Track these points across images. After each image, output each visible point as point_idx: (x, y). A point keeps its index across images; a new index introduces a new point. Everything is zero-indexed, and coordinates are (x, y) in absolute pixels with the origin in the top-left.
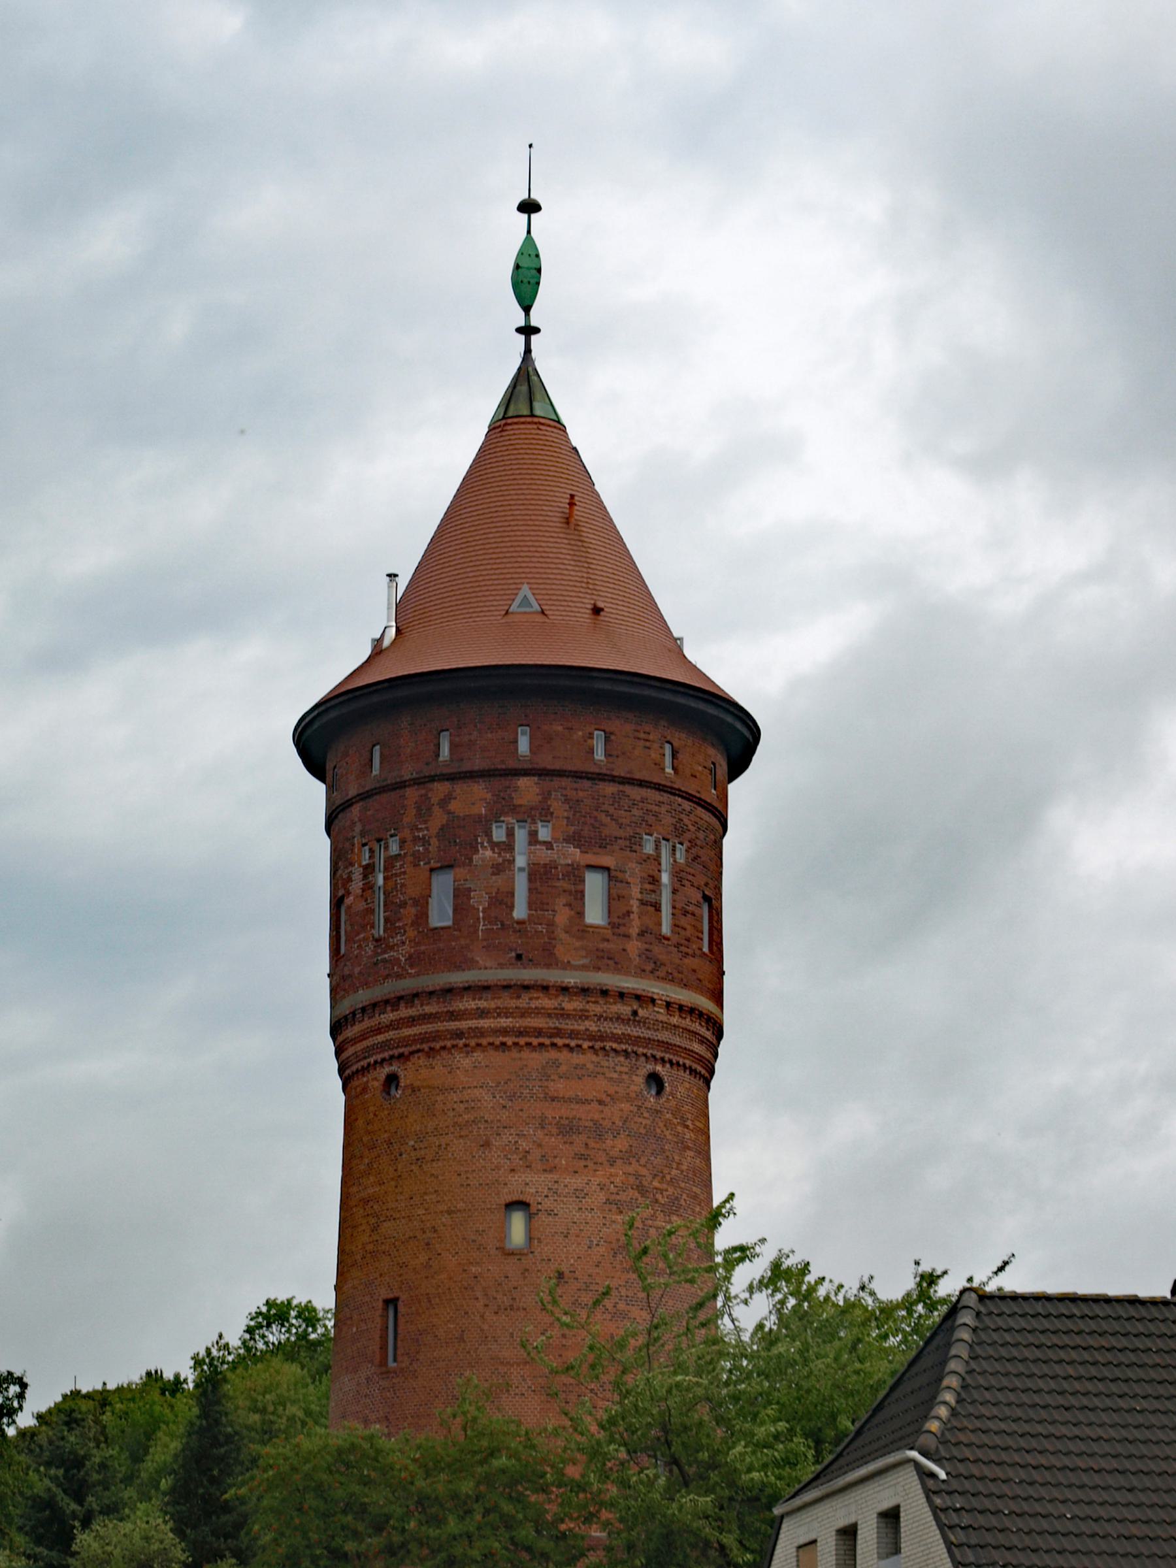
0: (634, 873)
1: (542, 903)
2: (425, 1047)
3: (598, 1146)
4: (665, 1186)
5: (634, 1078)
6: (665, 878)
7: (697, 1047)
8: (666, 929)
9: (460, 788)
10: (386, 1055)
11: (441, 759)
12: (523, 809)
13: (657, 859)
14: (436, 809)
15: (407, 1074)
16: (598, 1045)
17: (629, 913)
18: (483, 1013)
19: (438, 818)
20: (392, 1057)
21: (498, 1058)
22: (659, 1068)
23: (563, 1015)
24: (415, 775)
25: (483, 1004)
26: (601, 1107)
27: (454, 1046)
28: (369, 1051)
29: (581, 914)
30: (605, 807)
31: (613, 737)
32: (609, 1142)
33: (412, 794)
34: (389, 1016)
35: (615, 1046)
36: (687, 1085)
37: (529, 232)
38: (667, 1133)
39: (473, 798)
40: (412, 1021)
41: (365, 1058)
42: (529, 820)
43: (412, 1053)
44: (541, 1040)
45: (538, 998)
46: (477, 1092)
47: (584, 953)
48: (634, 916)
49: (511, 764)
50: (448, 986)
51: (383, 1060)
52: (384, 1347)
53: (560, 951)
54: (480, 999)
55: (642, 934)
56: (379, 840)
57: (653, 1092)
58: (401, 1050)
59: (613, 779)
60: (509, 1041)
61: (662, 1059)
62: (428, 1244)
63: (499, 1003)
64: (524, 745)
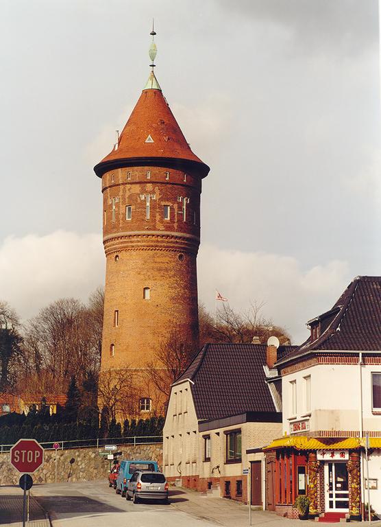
0: (176, 206)
9: (133, 186)
18: (138, 242)
19: (128, 194)
23: (158, 241)
33: (122, 187)
52: (115, 322)
59: (171, 184)
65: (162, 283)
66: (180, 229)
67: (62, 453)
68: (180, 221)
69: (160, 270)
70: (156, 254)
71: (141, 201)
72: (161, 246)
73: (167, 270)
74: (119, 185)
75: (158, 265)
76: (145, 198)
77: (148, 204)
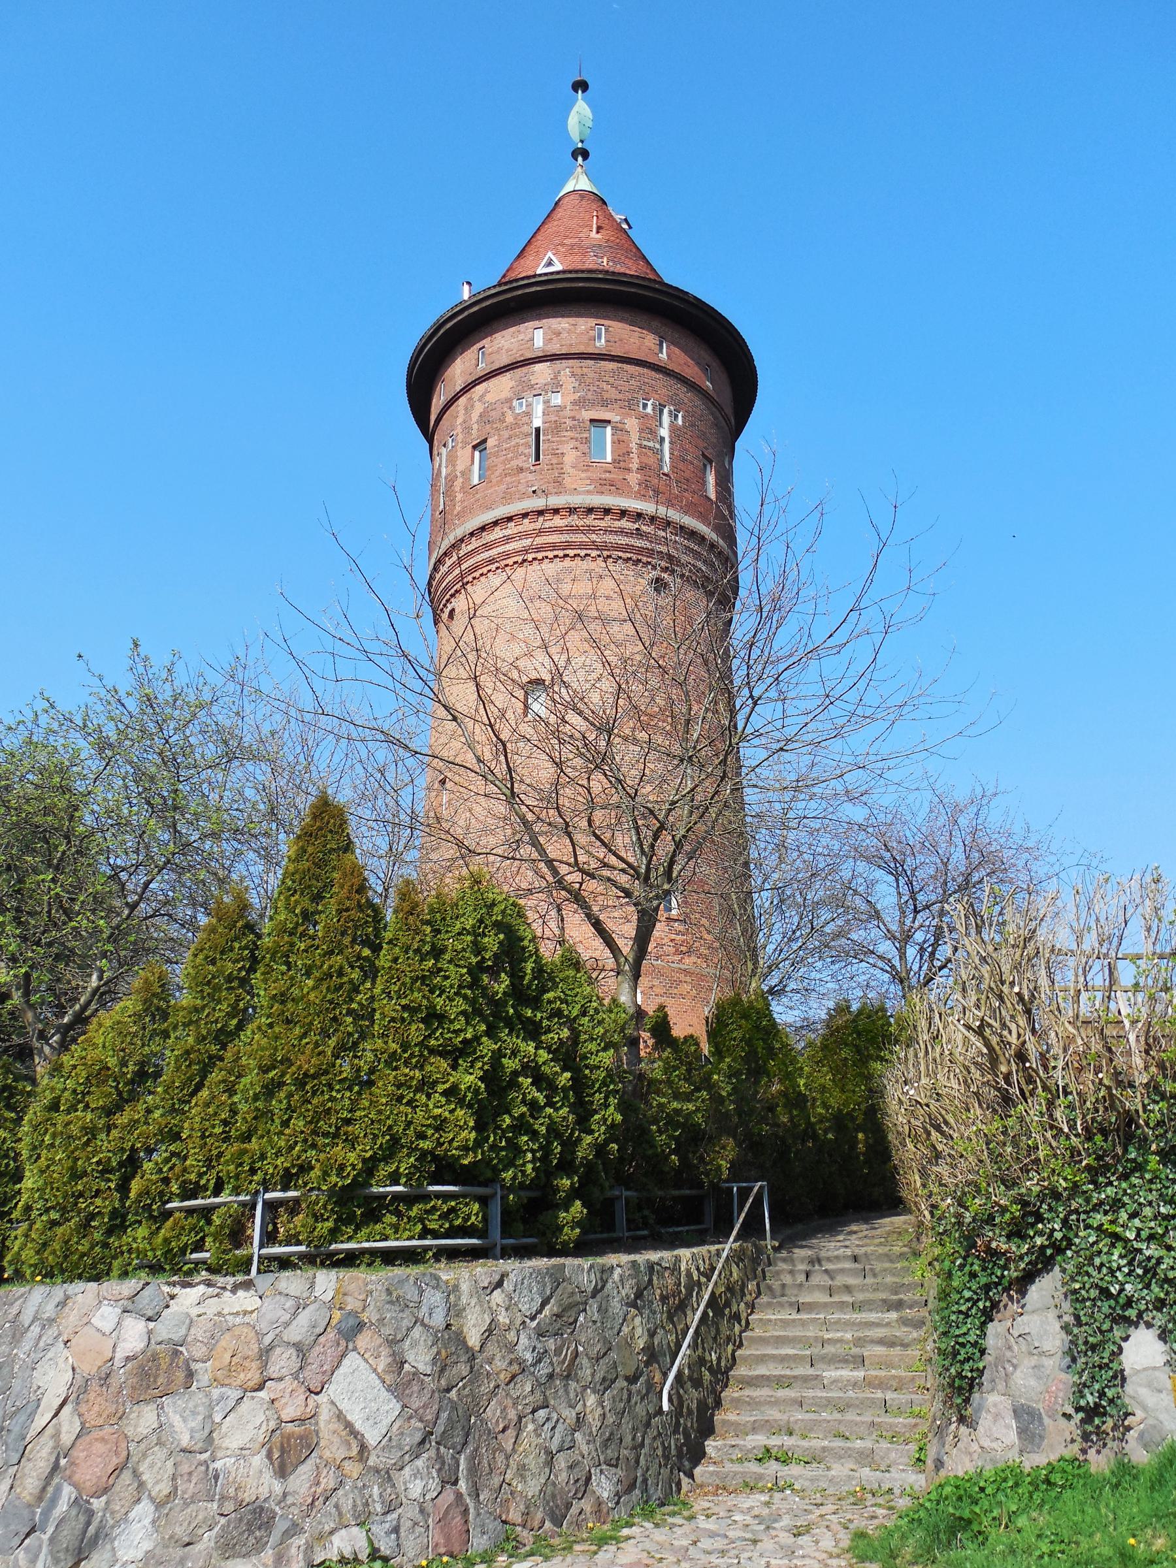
0: (632, 424)
4: (1138, 1094)
5: (640, 580)
17: (628, 453)
18: (508, 539)
30: (606, 379)
35: (620, 554)
39: (503, 385)
44: (556, 553)
47: (588, 482)
49: (529, 355)
53: (567, 481)
55: (641, 469)
63: (520, 528)
66: (650, 489)
67: (942, 1473)
71: (516, 416)
72: (582, 545)
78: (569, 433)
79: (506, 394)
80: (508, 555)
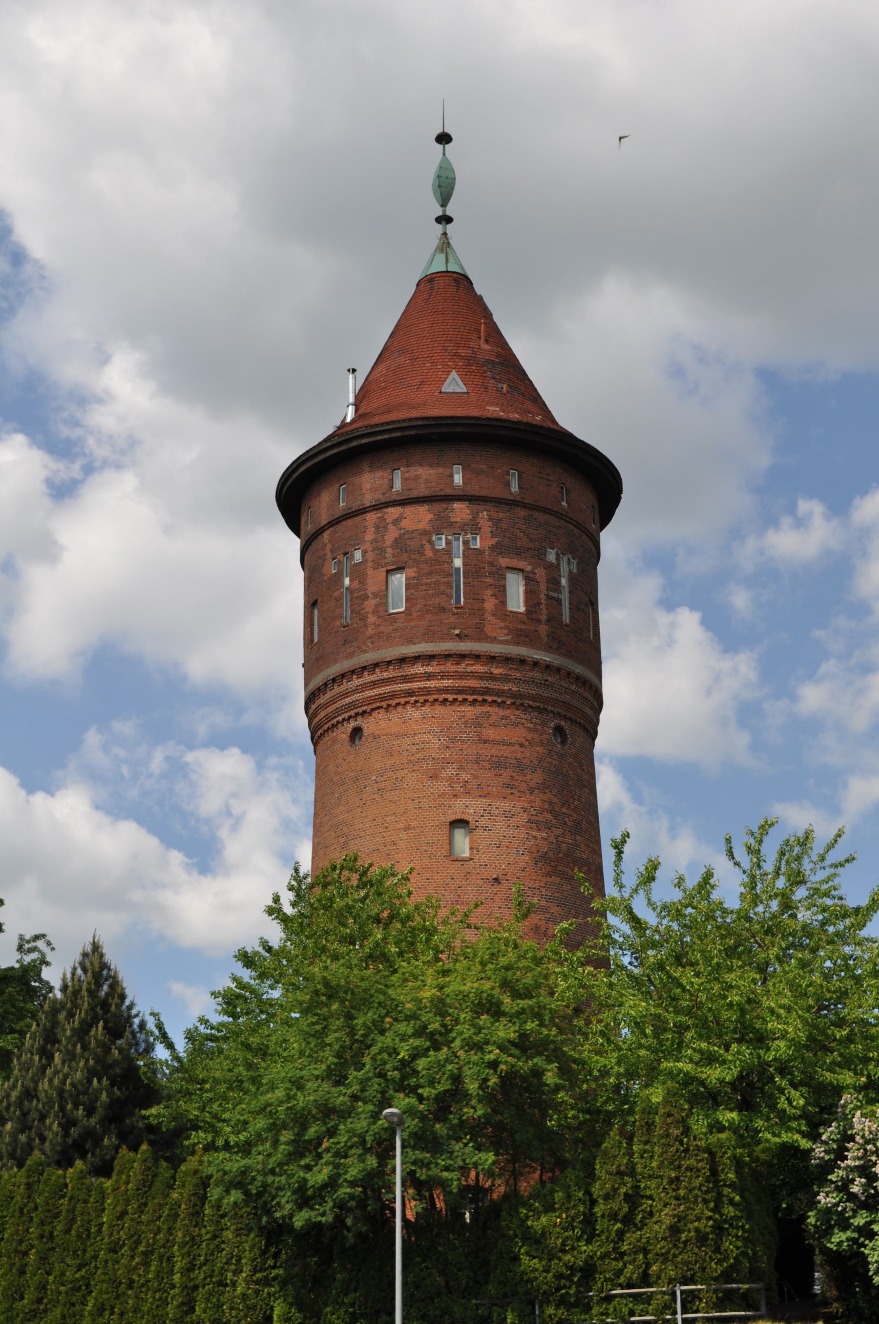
0: (541, 574)
1: (474, 594)
2: (384, 704)
3: (520, 778)
5: (545, 728)
6: (564, 582)
7: (587, 710)
8: (566, 618)
9: (409, 510)
10: (352, 713)
11: (394, 490)
12: (458, 525)
13: (557, 567)
14: (390, 526)
15: (369, 725)
16: (518, 702)
18: (429, 676)
20: (357, 714)
21: (439, 710)
22: (563, 723)
23: (491, 677)
24: (374, 503)
25: (429, 669)
26: (522, 749)
27: (407, 703)
28: (338, 712)
29: (504, 603)
31: (524, 475)
32: (529, 776)
33: (371, 518)
34: (356, 682)
35: (531, 703)
36: (582, 739)
37: (444, 154)
38: (571, 772)
40: (374, 684)
41: (335, 717)
42: (463, 533)
43: (373, 710)
45: (472, 665)
46: (425, 737)
47: (506, 631)
48: (543, 607)
49: (449, 491)
50: (401, 656)
51: (350, 717)
53: (488, 629)
54: (427, 665)
55: (549, 620)
56: (345, 554)
57: (559, 740)
58: (364, 708)
59: (525, 506)
60: (450, 697)
61: (565, 716)
62: (389, 855)
63: (442, 668)
64: (458, 479)
65: (506, 805)
68: (554, 620)
69: (498, 765)
70: (488, 715)
72: (499, 693)
73: (520, 767)
74: (363, 511)
75: (494, 751)
76: (448, 543)
77: (458, 563)
78: (488, 580)
79: (424, 525)
80: (428, 691)
